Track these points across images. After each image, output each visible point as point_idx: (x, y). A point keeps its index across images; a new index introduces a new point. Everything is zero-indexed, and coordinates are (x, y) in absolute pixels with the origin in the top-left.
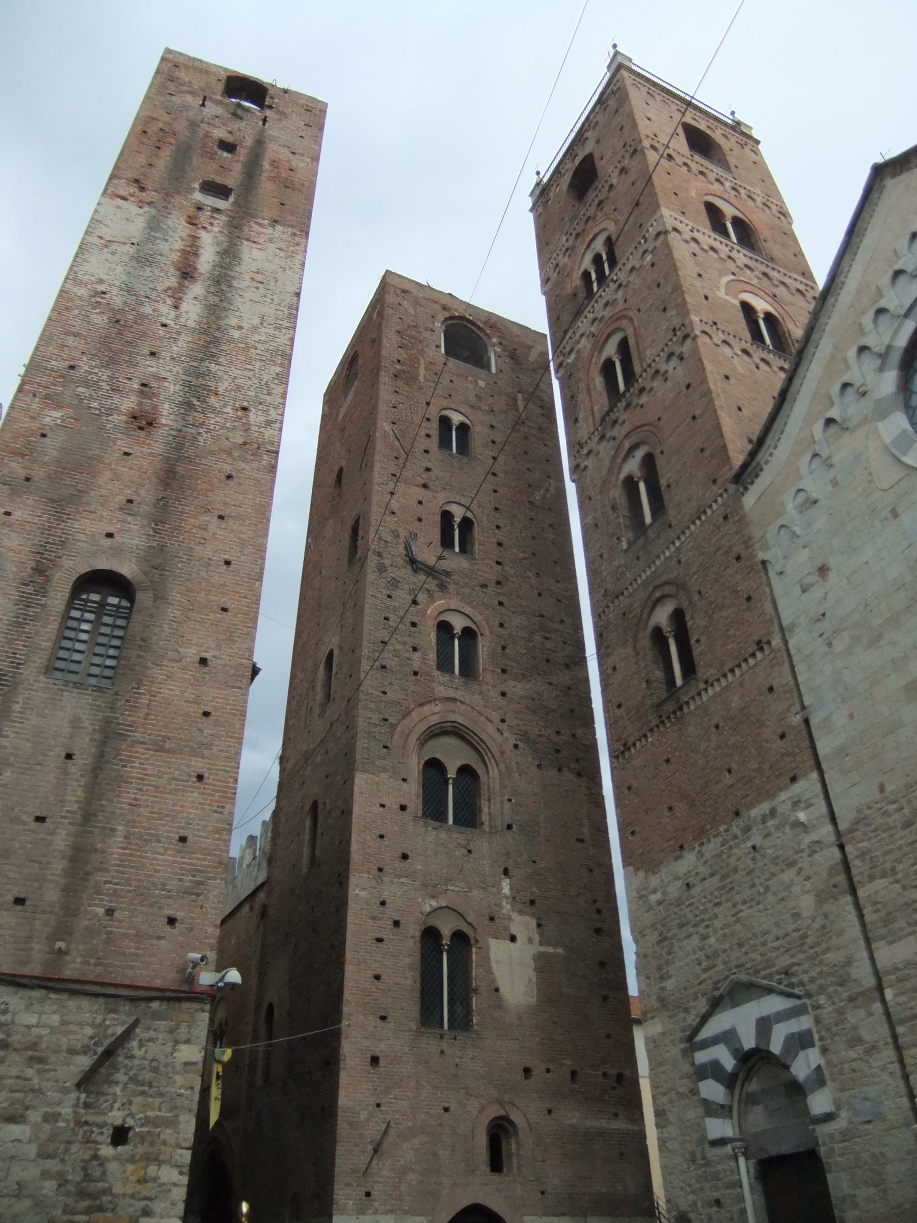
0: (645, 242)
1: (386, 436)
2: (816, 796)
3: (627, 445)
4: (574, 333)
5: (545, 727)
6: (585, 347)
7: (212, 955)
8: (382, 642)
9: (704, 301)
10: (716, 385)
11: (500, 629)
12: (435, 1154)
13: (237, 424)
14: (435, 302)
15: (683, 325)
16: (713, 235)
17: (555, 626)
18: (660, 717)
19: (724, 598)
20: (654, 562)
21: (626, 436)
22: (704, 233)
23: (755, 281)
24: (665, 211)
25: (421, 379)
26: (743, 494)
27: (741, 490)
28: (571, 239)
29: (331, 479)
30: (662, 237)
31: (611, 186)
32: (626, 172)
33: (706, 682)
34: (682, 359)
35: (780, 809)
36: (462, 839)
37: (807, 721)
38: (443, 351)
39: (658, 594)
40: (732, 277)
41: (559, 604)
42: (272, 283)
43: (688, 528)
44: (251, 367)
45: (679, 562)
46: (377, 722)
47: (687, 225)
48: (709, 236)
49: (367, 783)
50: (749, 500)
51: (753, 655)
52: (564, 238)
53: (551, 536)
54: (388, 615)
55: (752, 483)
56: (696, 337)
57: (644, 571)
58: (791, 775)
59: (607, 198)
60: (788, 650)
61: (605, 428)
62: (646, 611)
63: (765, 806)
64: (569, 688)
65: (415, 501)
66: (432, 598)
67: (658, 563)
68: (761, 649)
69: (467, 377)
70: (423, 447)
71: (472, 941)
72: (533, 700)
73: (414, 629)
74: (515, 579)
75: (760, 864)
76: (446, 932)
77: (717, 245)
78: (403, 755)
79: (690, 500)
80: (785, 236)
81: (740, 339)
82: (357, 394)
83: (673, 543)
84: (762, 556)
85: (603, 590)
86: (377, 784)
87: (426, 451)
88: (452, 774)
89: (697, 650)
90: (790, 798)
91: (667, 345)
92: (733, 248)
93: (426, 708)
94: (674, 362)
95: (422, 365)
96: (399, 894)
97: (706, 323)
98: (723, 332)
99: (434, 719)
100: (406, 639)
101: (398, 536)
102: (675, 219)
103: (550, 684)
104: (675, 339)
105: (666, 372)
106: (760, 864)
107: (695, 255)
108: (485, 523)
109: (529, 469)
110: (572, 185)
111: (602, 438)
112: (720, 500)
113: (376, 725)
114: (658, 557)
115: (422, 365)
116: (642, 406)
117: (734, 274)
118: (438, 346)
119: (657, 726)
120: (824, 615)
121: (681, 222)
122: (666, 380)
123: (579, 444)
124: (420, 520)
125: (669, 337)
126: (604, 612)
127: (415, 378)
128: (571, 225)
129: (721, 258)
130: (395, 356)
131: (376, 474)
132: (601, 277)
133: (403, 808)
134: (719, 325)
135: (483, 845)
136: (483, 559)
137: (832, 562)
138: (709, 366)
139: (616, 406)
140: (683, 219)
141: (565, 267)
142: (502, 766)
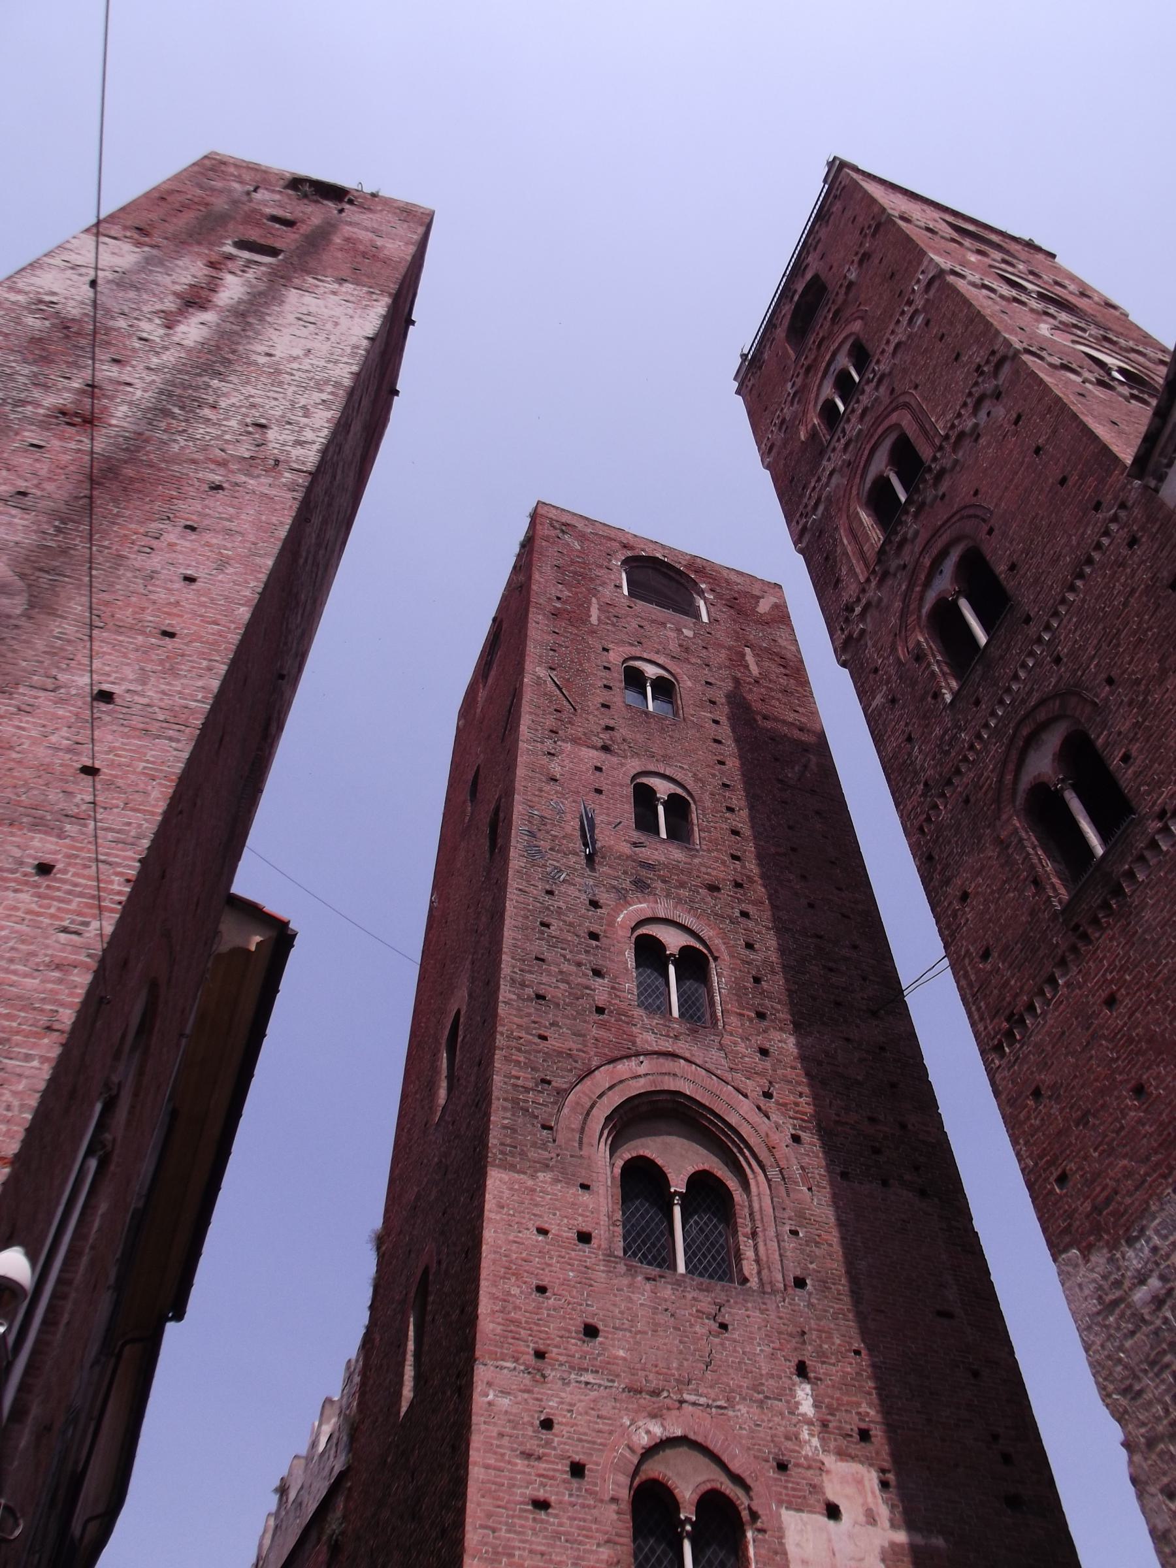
1: (539, 682)
25: (594, 620)
36: (706, 1302)
38: (626, 592)
46: (531, 1084)
49: (511, 1189)
64: (882, 1049)
72: (820, 1063)
73: (594, 943)
86: (533, 1190)
96: (580, 1407)
100: (583, 957)
103: (848, 1040)
113: (527, 1090)
118: (619, 587)
124: (599, 791)
131: (523, 728)
142: (773, 1173)
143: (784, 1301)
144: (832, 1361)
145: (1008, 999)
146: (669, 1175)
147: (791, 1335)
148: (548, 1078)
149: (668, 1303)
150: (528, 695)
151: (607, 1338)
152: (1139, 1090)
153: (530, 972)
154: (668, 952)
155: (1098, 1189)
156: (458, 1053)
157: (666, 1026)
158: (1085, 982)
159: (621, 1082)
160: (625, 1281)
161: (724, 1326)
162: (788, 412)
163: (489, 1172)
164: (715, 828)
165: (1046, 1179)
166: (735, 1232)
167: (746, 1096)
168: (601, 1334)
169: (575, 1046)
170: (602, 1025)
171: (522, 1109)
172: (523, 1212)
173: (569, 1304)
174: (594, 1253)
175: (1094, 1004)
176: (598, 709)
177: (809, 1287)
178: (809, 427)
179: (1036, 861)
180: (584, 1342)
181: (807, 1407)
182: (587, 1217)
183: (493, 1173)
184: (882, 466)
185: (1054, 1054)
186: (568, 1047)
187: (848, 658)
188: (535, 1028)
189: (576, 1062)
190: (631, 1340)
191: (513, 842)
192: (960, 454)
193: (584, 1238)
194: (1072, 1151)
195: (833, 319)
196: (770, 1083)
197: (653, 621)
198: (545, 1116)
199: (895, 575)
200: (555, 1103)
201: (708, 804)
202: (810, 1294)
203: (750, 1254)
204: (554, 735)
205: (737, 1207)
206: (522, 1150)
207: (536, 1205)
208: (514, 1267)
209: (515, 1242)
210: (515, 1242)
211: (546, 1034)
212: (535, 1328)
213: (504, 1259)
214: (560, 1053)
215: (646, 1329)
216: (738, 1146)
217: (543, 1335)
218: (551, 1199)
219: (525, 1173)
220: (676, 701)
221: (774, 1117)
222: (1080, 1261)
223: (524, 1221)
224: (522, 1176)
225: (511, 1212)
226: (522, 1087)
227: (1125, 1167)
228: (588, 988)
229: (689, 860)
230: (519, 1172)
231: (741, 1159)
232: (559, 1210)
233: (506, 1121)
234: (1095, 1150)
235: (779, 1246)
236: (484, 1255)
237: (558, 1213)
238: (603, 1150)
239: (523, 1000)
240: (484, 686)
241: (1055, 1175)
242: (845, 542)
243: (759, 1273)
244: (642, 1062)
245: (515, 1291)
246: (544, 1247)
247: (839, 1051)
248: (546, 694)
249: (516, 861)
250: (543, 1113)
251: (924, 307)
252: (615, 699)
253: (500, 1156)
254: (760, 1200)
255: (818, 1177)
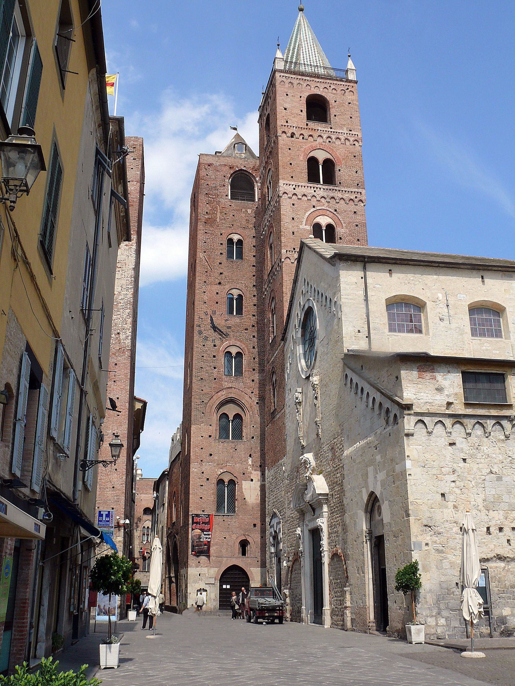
7: (123, 516)
12: (221, 551)
13: (116, 341)
14: (226, 165)
25: (218, 220)
36: (233, 445)
38: (230, 198)
42: (124, 266)
44: (119, 313)
71: (236, 483)
76: (226, 480)
96: (208, 469)
99: (223, 398)
108: (248, 295)
133: (210, 436)
135: (242, 446)
170: (216, 383)
181: (250, 463)
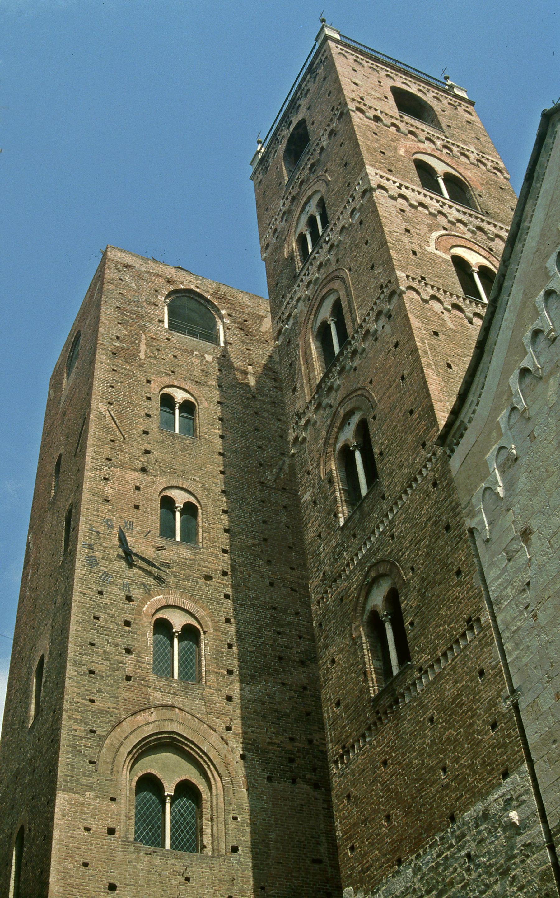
0: (353, 200)
1: (101, 417)
2: (527, 792)
3: (342, 413)
4: (291, 298)
5: (277, 734)
6: (302, 311)
8: (91, 644)
9: (412, 256)
10: (423, 342)
11: (226, 625)
15: (390, 282)
16: (423, 191)
17: (289, 619)
18: (378, 713)
19: (436, 573)
20: (369, 538)
21: (339, 405)
22: (413, 190)
23: (469, 235)
24: (370, 170)
25: (142, 355)
26: (450, 457)
27: (448, 452)
28: (288, 203)
29: (51, 468)
30: (367, 195)
31: (322, 149)
32: (335, 134)
33: (420, 670)
34: (389, 317)
35: (492, 811)
36: (179, 865)
37: (516, 706)
38: (166, 325)
39: (373, 574)
40: (444, 232)
41: (294, 593)
43: (400, 498)
45: (392, 537)
46: (84, 734)
47: (394, 182)
48: (419, 193)
49: (70, 804)
50: (455, 463)
51: (464, 635)
52: (282, 202)
53: (284, 519)
54: (97, 614)
55: (457, 444)
56: (402, 293)
57: (360, 549)
58: (502, 769)
59: (318, 160)
60: (497, 628)
61: (320, 396)
62: (363, 593)
63: (480, 806)
64: (305, 688)
65: (132, 486)
66: (148, 594)
67: (373, 539)
68: (471, 628)
69: (192, 352)
70: (142, 428)
72: (263, 703)
73: (127, 628)
74: (242, 569)
75: (474, 875)
77: (427, 201)
78: (112, 771)
79: (401, 467)
80: (501, 191)
81: (451, 295)
82: (78, 374)
83: (387, 516)
84: (470, 523)
85: (322, 575)
86: (82, 804)
87: (146, 433)
88: (169, 790)
89: (410, 634)
90: (501, 797)
91: (375, 303)
92: (444, 204)
93: (139, 718)
94: (383, 320)
95: (144, 341)
97: (413, 279)
98: (432, 287)
100: (119, 640)
101: (111, 526)
102: (382, 177)
103: (283, 684)
104: (382, 296)
105: (376, 331)
106: (474, 875)
107: (403, 211)
109: (260, 447)
110: (288, 151)
111: (319, 406)
112: (429, 465)
113: (81, 738)
114: (373, 532)
115: (144, 341)
116: (355, 369)
117: (445, 229)
118: (161, 321)
119: (375, 724)
120: (528, 584)
121: (388, 180)
122: (376, 340)
123: (297, 415)
124: (137, 507)
125: (377, 295)
126: (322, 598)
127: (135, 356)
128: (287, 189)
129: (431, 214)
130: (115, 333)
131: (88, 459)
132: (316, 238)
134: (428, 281)
136: (207, 548)
137: (534, 525)
138: (415, 322)
139: (331, 372)
140: (390, 177)
141: (282, 232)
142: (227, 780)
143: (224, 861)
144: (247, 895)
145: (344, 736)
146: (164, 785)
147: (225, 881)
148: (94, 729)
149: (157, 868)
150: (93, 429)
151: (121, 891)
152: (388, 817)
153: (86, 654)
154: (174, 630)
155: (365, 861)
156: (42, 688)
157: (169, 686)
158: (377, 746)
159: (139, 727)
160: (134, 856)
161: (187, 879)
162: (281, 225)
163: (57, 794)
164: (214, 528)
165: (346, 846)
166: (201, 817)
167: (215, 731)
168: (118, 888)
169: (111, 705)
170: (130, 689)
171: (78, 751)
172: (77, 818)
173: (101, 872)
174: (116, 840)
175: (378, 760)
176: (140, 436)
177: (240, 852)
178: (290, 248)
179: (368, 660)
180: (108, 893)
182: (114, 818)
183: (60, 795)
184: (328, 314)
185: (358, 780)
186: (107, 706)
187: (296, 451)
188: (87, 695)
189: (112, 716)
190: (134, 891)
191: (78, 556)
192: (367, 344)
193: (111, 831)
194: (358, 836)
195: (311, 169)
196: (231, 720)
197: (184, 351)
198: (91, 755)
199: (325, 409)
200: (98, 746)
201: (210, 509)
202: (240, 855)
203: (207, 830)
204: (109, 462)
205: (203, 802)
206: (77, 778)
207: (85, 813)
208: (71, 852)
209: (71, 837)
210: (71, 837)
211: (94, 698)
212: (81, 887)
213: (65, 847)
214: (101, 711)
215: (143, 884)
216: (207, 764)
217: (86, 891)
218: (93, 809)
219: (78, 793)
220: (196, 420)
221: (231, 744)
222: (353, 894)
223: (77, 824)
224: (77, 795)
225: (70, 819)
226: (79, 736)
227: (376, 855)
228: (121, 662)
229: (192, 557)
230: (75, 793)
231: (208, 772)
232: (97, 815)
233: (68, 760)
234: (367, 841)
235: (225, 827)
236: (53, 846)
237: (97, 817)
238: (125, 772)
239: (81, 675)
240: (68, 375)
241: (349, 846)
242: (302, 363)
243: (212, 843)
244: (152, 713)
245: (71, 866)
246: (88, 839)
247: (277, 693)
248: (105, 427)
249: (80, 570)
250: (90, 753)
251: (360, 208)
252: (152, 426)
253: (64, 783)
254: (217, 798)
255: (253, 781)
